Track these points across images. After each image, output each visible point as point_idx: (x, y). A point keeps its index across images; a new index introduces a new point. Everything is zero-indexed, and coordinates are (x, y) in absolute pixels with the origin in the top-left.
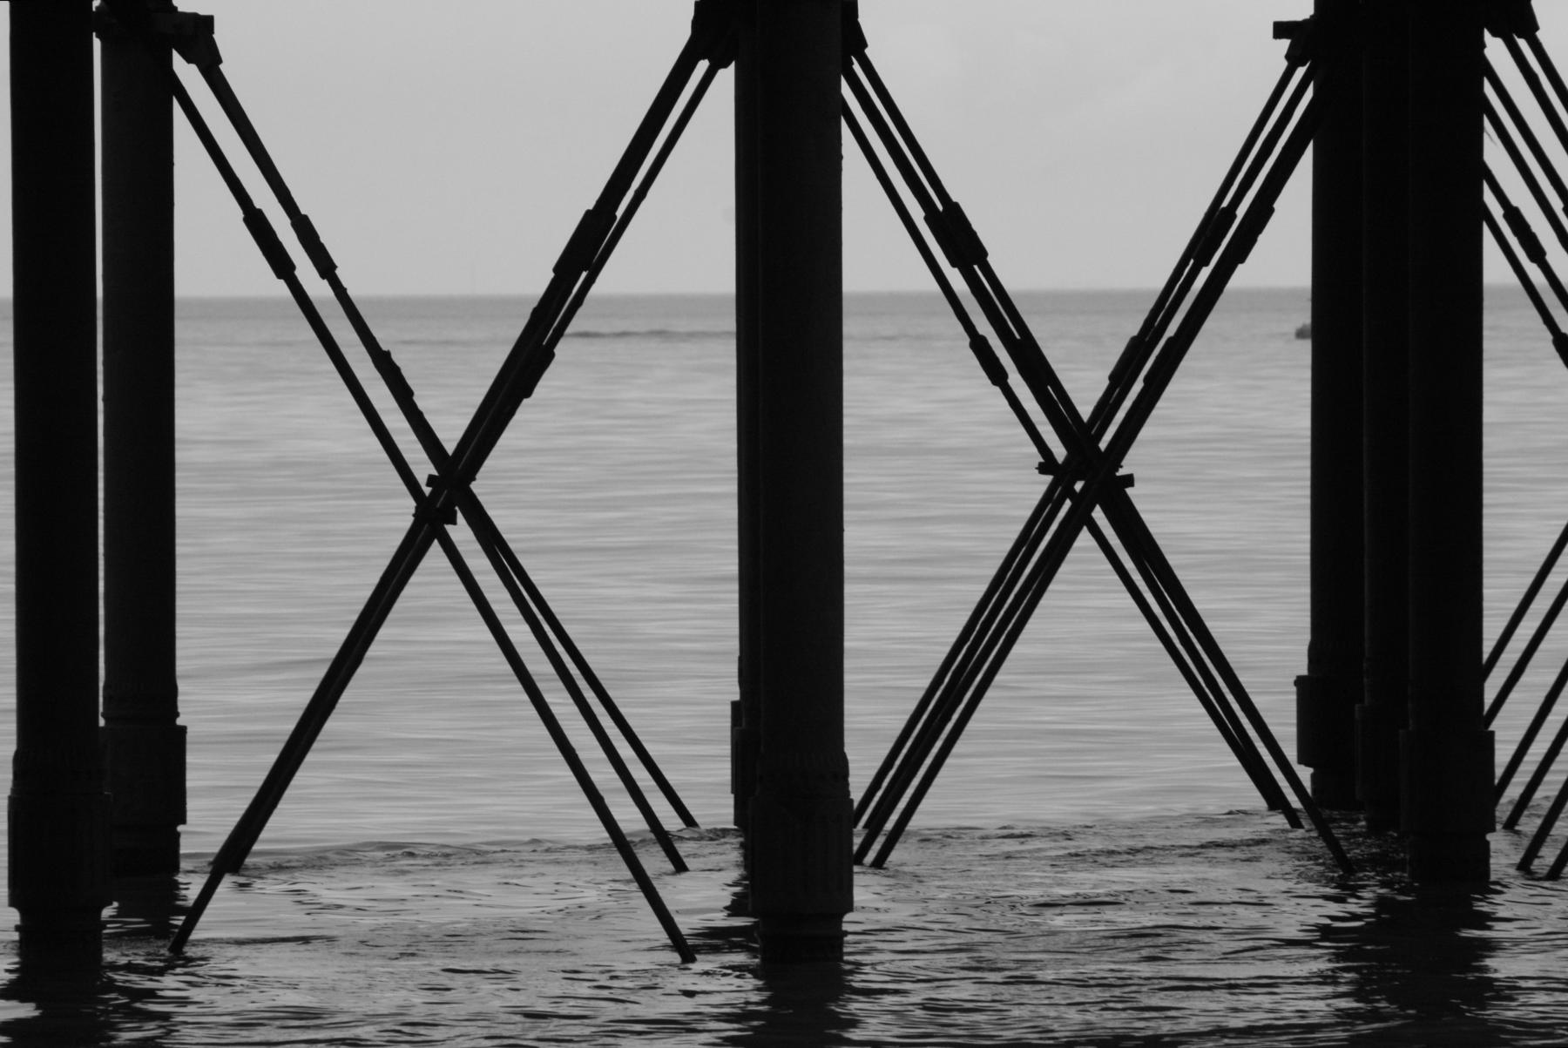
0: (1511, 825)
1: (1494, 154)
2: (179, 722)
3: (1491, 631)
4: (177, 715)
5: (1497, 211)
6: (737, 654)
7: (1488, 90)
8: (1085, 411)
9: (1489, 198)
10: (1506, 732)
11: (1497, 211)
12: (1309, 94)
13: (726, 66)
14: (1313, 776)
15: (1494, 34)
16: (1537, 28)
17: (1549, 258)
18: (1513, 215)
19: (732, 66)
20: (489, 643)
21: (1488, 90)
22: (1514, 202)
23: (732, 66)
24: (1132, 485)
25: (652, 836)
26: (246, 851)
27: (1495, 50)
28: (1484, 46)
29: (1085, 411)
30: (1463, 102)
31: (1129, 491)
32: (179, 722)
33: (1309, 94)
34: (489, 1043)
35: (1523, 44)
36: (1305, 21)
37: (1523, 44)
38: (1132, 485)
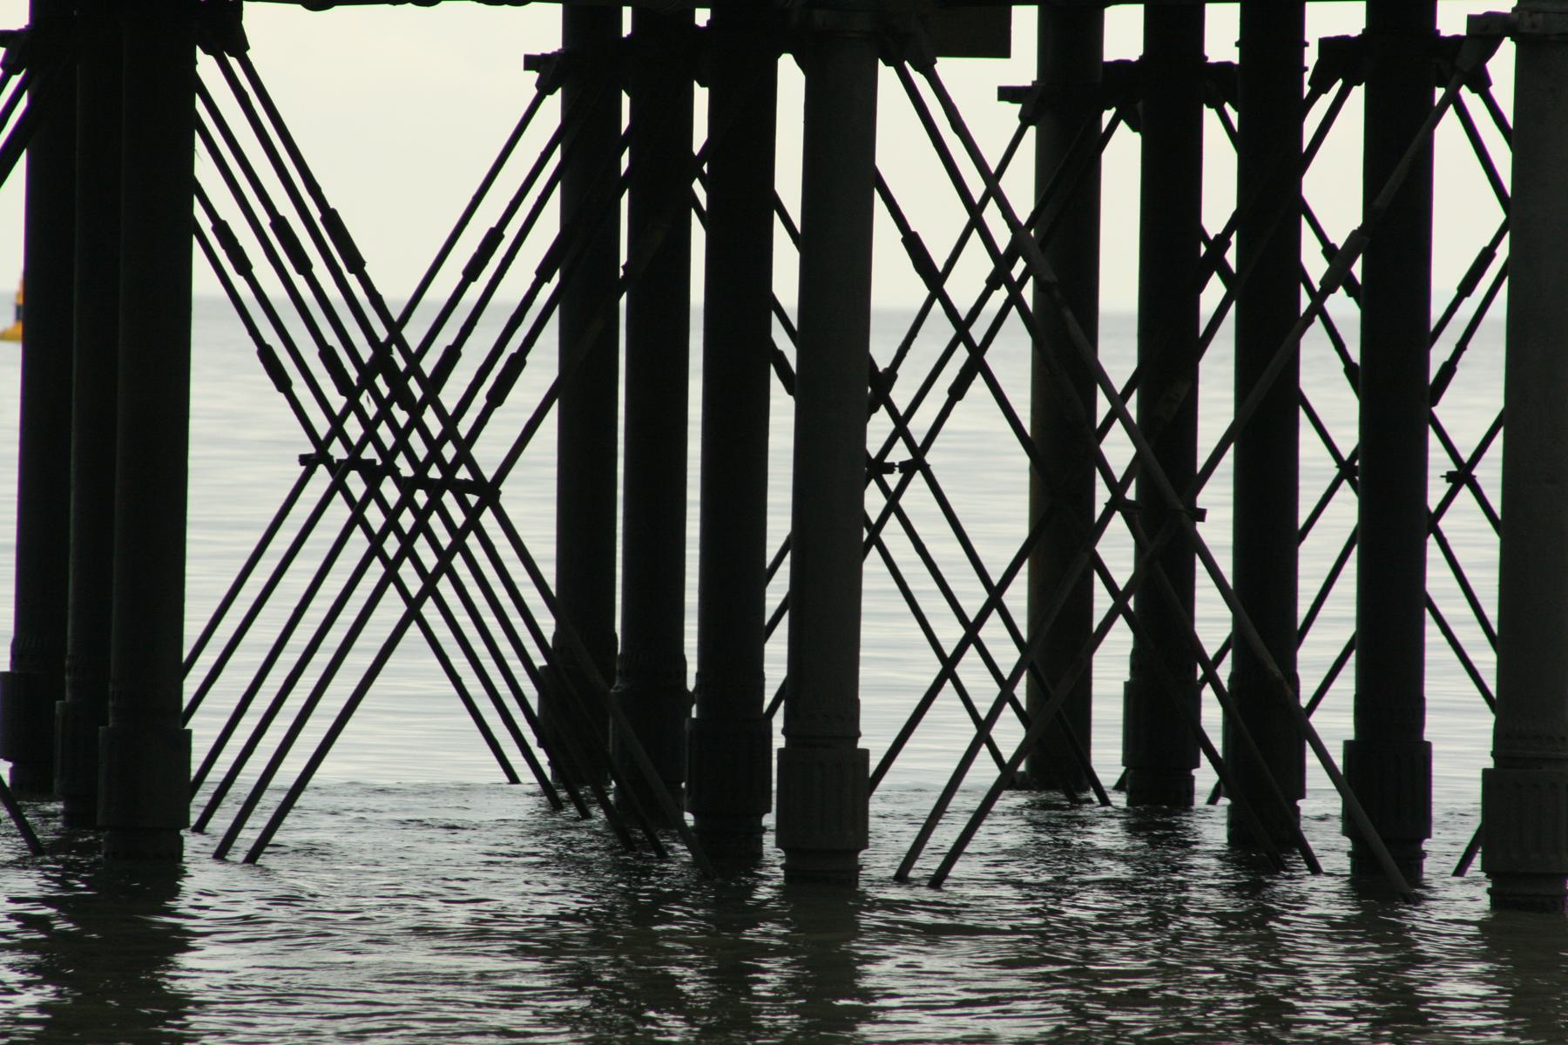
0: (200, 828)
1: (204, 170)
2: (861, 744)
3: (192, 630)
4: (858, 735)
5: (205, 224)
6: (1353, 693)
7: (200, 106)
8: (900, 439)
9: (199, 212)
10: (203, 729)
11: (205, 224)
12: (23, 103)
13: (552, 92)
14: (12, 771)
15: (206, 52)
16: (248, 48)
17: (1466, 300)
18: (222, 229)
19: (559, 92)
20: (978, 665)
21: (200, 106)
22: (223, 216)
23: (559, 92)
24: (1202, 519)
25: (1483, 875)
26: (946, 877)
27: (206, 67)
28: (195, 63)
29: (900, 439)
30: (174, 118)
31: (1200, 526)
32: (861, 744)
33: (23, 103)
34: (300, 1040)
35: (233, 62)
36: (20, 31)
37: (233, 62)
38: (1202, 519)
